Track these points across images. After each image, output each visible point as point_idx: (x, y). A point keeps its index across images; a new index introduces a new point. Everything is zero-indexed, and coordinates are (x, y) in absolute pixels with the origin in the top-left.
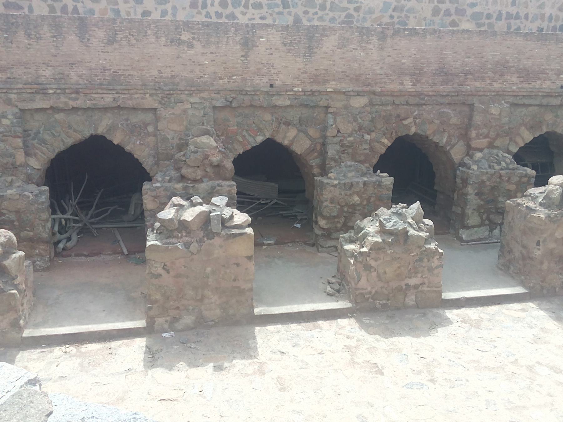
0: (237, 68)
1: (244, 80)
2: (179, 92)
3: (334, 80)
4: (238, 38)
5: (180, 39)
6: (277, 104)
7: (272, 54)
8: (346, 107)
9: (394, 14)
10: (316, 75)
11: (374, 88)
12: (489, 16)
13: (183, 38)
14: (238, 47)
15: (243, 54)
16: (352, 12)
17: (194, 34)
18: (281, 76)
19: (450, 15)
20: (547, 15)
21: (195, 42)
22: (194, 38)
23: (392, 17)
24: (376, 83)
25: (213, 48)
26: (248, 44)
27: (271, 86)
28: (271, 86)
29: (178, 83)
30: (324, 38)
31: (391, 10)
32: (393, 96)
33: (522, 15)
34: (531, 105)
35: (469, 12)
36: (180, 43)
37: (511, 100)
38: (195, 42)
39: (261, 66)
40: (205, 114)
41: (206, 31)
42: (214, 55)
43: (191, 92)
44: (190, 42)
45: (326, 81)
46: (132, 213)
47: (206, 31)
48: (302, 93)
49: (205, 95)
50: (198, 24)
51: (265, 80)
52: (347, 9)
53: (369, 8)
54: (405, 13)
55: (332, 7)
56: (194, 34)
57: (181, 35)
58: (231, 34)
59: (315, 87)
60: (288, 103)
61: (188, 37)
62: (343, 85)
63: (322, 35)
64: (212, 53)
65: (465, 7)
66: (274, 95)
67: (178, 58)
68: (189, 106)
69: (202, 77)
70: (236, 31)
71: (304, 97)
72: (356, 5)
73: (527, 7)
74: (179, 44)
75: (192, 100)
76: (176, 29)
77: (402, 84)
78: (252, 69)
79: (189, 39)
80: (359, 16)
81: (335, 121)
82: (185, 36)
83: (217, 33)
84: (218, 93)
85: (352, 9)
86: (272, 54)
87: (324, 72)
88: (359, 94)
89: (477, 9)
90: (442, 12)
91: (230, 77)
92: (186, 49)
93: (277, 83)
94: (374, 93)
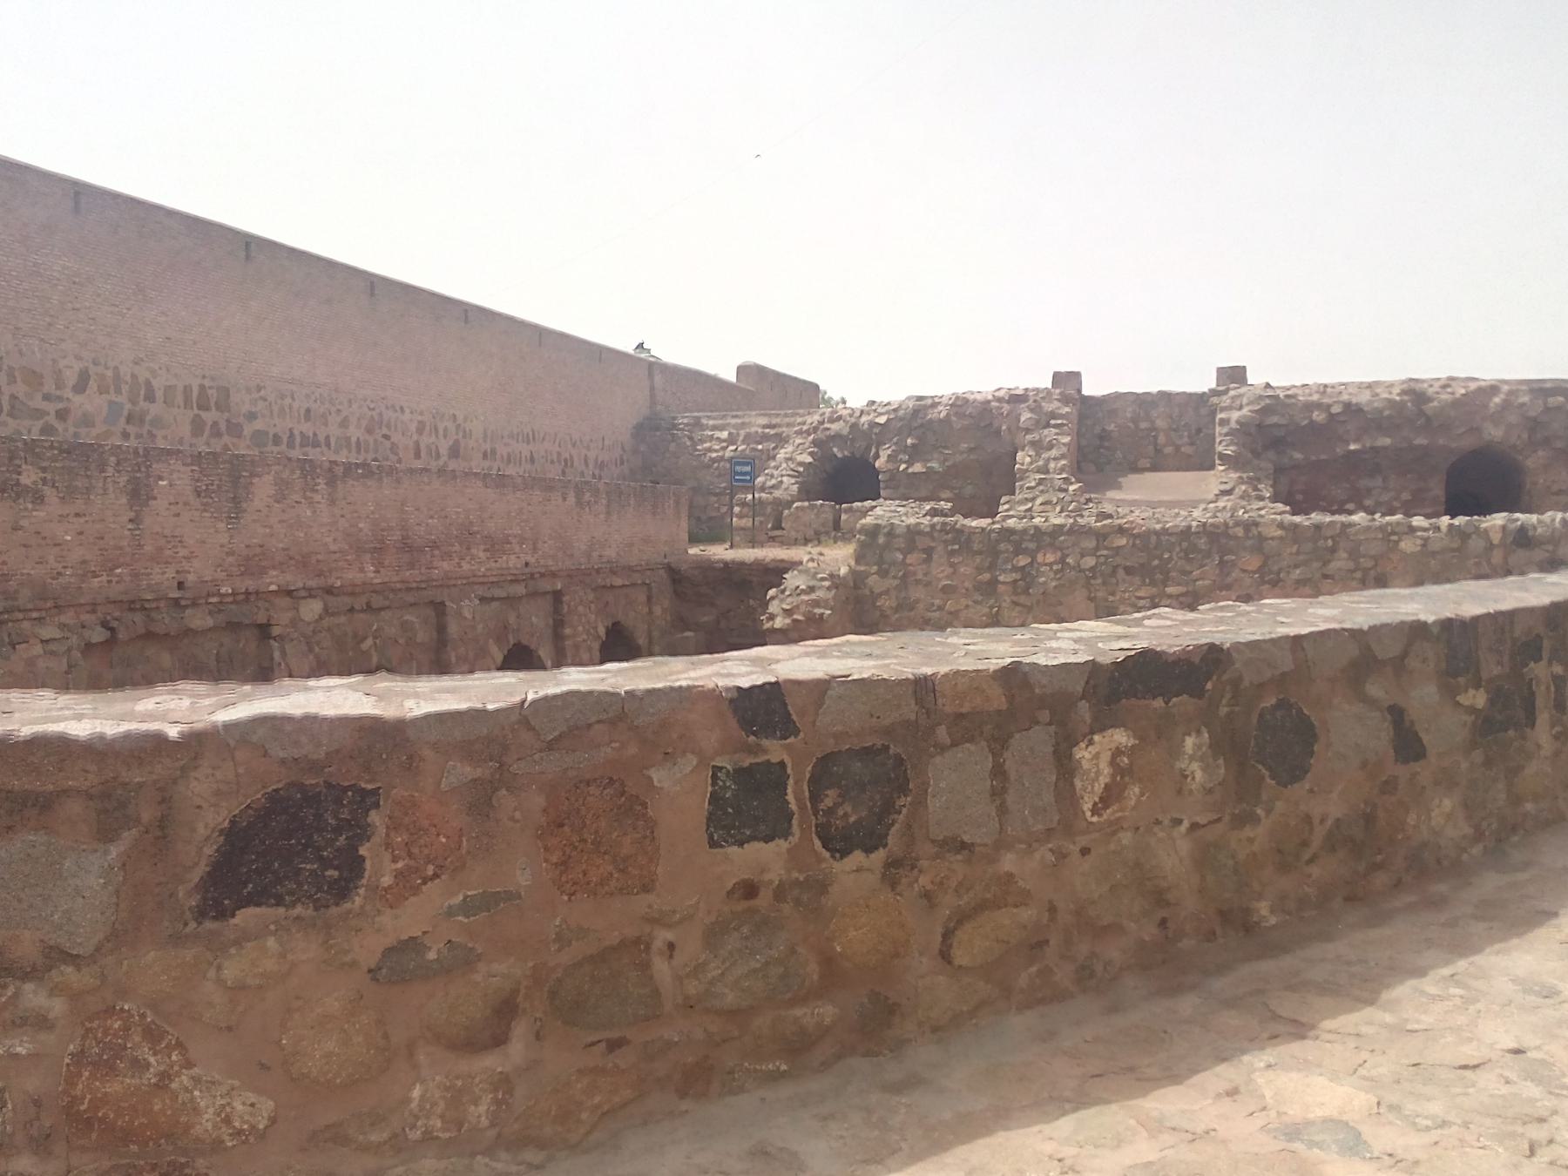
0: (121, 548)
1: (136, 575)
2: (20, 616)
3: (274, 568)
4: (123, 480)
5: (18, 484)
6: (192, 626)
7: (178, 515)
8: (294, 623)
9: (131, 429)
10: (248, 559)
11: (330, 582)
12: (277, 440)
13: (25, 480)
14: (124, 500)
15: (132, 515)
16: (51, 419)
17: (44, 470)
18: (196, 563)
19: (218, 435)
20: (354, 440)
21: (47, 491)
22: (44, 481)
23: (126, 435)
24: (330, 571)
25: (79, 505)
26: (139, 494)
27: (181, 585)
28: (181, 585)
29: (16, 592)
30: (255, 480)
31: (123, 420)
32: (353, 594)
33: (321, 438)
34: (493, 599)
35: (248, 430)
36: (19, 492)
37: (480, 591)
38: (47, 491)
39: (162, 542)
40: (70, 666)
41: (67, 463)
42: (82, 520)
43: (44, 614)
44: (37, 491)
45: (263, 571)
46: (1561, 399)
47: (67, 463)
48: (230, 599)
49: (68, 618)
50: (52, 447)
51: (171, 573)
52: (44, 413)
53: (84, 415)
54: (147, 427)
55: (13, 407)
56: (44, 470)
57: (19, 474)
58: (110, 471)
59: (250, 584)
60: (210, 622)
61: (34, 478)
62: (289, 577)
63: (252, 475)
64: (77, 515)
65: (241, 420)
66: (186, 607)
67: (15, 529)
68: (38, 649)
69: (59, 574)
70: (118, 464)
71: (233, 607)
72: (60, 406)
73: (326, 424)
74: (18, 496)
75: (48, 632)
76: (11, 459)
77: (362, 570)
78: (148, 548)
79: (35, 483)
80: (66, 430)
81: (284, 653)
82: (29, 477)
83: (87, 469)
84: (94, 612)
85: (53, 413)
86: (178, 515)
87: (258, 550)
88: (311, 594)
89: (258, 425)
90: (208, 428)
91: (111, 570)
92: (30, 506)
93: (191, 578)
94: (329, 591)
